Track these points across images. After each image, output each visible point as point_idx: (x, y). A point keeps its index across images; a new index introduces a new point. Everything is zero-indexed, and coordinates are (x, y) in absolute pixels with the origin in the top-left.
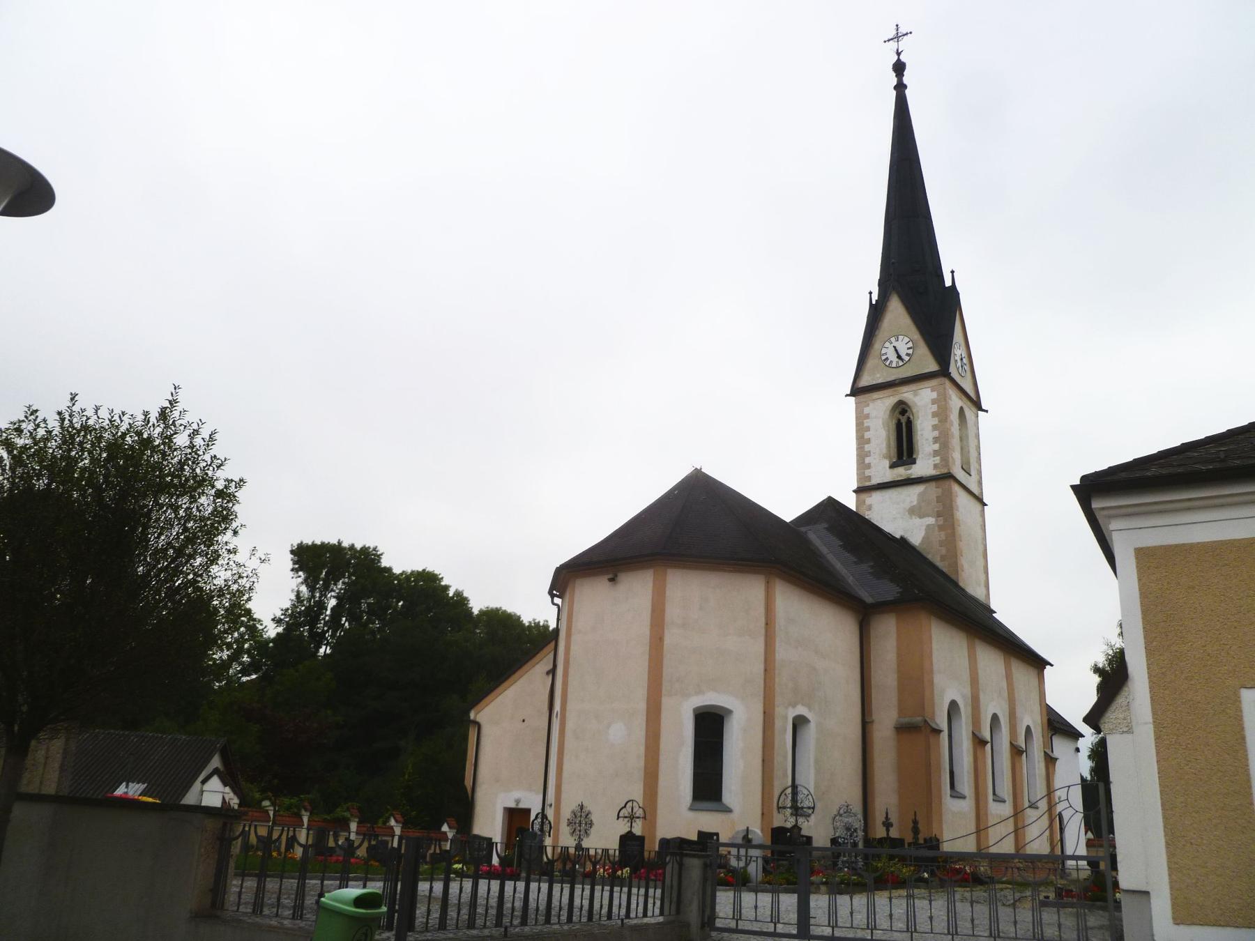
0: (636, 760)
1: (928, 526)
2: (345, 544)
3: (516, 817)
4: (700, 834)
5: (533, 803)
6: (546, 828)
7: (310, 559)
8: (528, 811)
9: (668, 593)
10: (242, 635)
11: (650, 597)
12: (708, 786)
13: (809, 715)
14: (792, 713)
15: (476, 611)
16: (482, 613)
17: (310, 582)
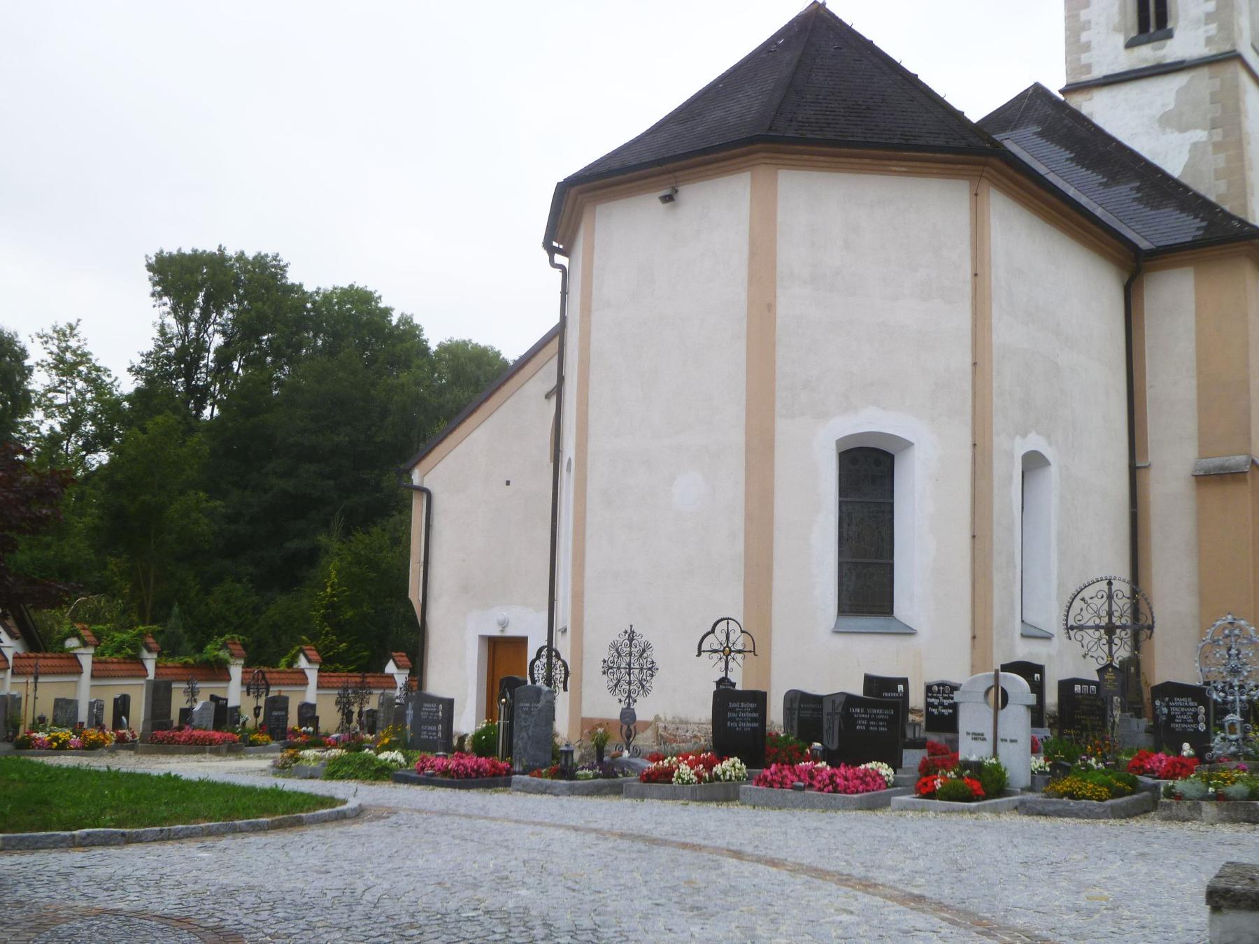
0: (729, 543)
1: (1195, 146)
2: (231, 252)
3: (502, 651)
4: (870, 681)
5: (530, 626)
6: (558, 674)
7: (180, 277)
8: (522, 642)
9: (780, 218)
10: (81, 393)
11: (745, 227)
12: (866, 584)
13: (1048, 452)
14: (1022, 447)
15: (433, 346)
16: (443, 348)
17: (182, 312)
